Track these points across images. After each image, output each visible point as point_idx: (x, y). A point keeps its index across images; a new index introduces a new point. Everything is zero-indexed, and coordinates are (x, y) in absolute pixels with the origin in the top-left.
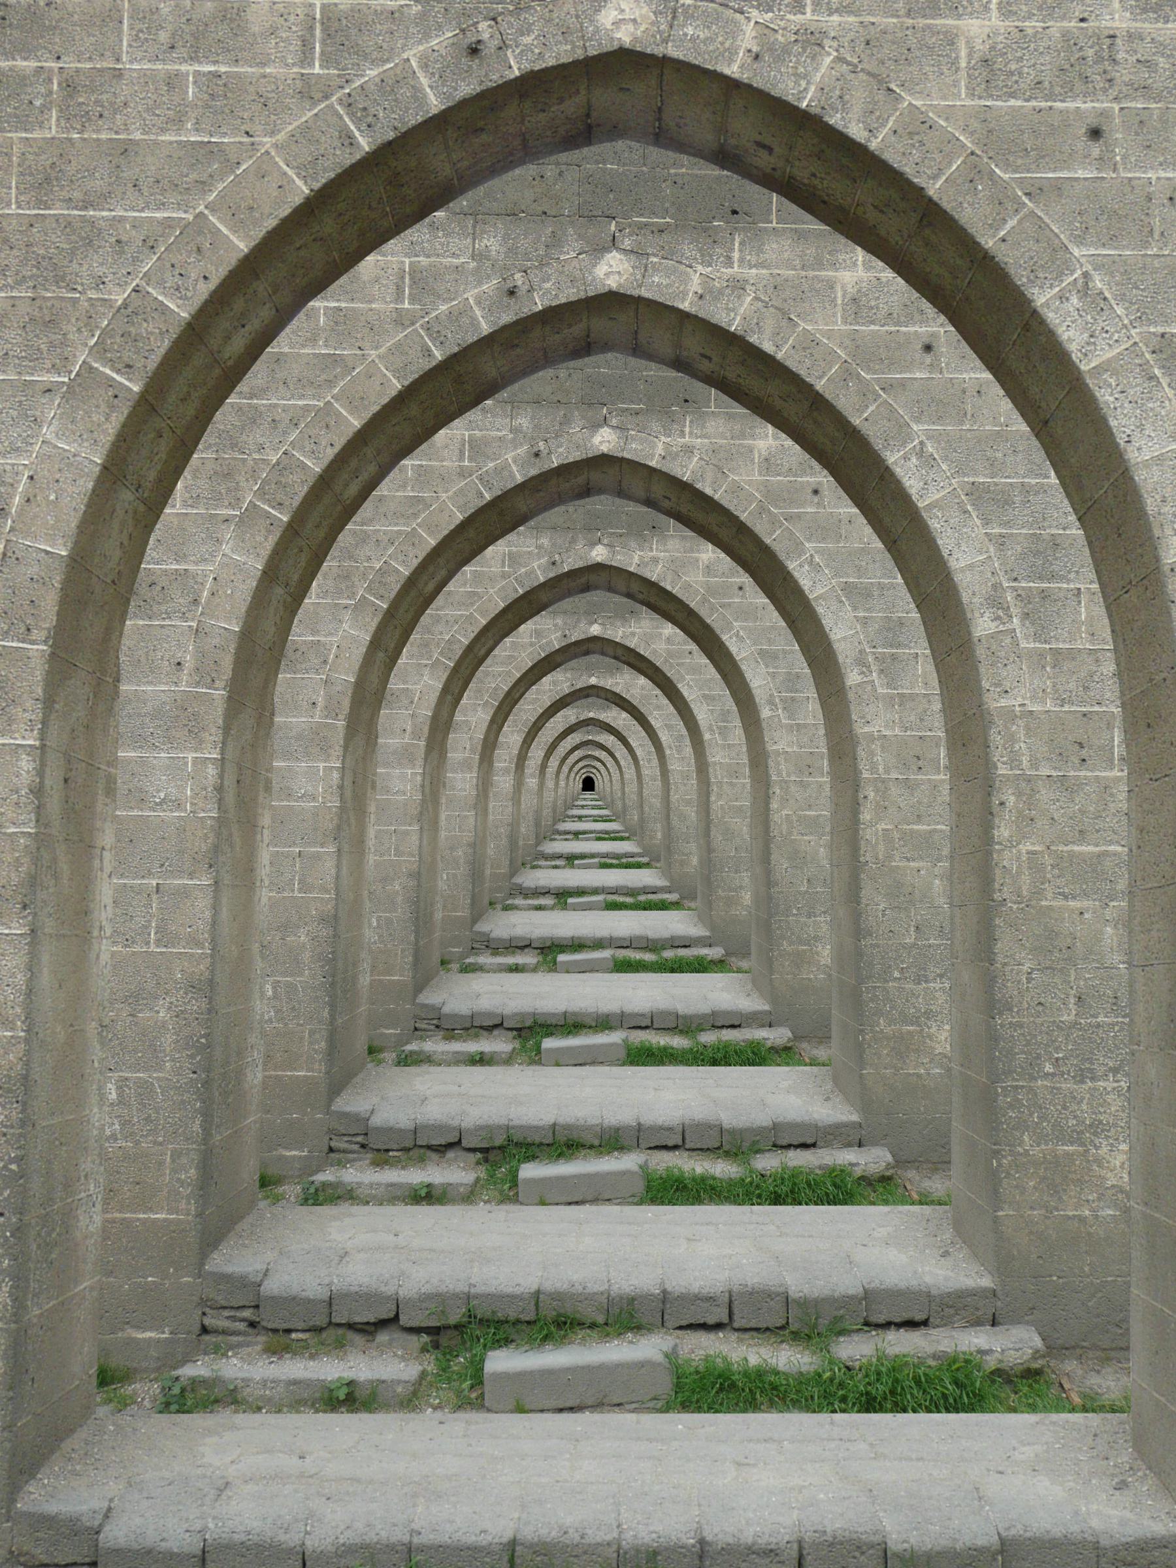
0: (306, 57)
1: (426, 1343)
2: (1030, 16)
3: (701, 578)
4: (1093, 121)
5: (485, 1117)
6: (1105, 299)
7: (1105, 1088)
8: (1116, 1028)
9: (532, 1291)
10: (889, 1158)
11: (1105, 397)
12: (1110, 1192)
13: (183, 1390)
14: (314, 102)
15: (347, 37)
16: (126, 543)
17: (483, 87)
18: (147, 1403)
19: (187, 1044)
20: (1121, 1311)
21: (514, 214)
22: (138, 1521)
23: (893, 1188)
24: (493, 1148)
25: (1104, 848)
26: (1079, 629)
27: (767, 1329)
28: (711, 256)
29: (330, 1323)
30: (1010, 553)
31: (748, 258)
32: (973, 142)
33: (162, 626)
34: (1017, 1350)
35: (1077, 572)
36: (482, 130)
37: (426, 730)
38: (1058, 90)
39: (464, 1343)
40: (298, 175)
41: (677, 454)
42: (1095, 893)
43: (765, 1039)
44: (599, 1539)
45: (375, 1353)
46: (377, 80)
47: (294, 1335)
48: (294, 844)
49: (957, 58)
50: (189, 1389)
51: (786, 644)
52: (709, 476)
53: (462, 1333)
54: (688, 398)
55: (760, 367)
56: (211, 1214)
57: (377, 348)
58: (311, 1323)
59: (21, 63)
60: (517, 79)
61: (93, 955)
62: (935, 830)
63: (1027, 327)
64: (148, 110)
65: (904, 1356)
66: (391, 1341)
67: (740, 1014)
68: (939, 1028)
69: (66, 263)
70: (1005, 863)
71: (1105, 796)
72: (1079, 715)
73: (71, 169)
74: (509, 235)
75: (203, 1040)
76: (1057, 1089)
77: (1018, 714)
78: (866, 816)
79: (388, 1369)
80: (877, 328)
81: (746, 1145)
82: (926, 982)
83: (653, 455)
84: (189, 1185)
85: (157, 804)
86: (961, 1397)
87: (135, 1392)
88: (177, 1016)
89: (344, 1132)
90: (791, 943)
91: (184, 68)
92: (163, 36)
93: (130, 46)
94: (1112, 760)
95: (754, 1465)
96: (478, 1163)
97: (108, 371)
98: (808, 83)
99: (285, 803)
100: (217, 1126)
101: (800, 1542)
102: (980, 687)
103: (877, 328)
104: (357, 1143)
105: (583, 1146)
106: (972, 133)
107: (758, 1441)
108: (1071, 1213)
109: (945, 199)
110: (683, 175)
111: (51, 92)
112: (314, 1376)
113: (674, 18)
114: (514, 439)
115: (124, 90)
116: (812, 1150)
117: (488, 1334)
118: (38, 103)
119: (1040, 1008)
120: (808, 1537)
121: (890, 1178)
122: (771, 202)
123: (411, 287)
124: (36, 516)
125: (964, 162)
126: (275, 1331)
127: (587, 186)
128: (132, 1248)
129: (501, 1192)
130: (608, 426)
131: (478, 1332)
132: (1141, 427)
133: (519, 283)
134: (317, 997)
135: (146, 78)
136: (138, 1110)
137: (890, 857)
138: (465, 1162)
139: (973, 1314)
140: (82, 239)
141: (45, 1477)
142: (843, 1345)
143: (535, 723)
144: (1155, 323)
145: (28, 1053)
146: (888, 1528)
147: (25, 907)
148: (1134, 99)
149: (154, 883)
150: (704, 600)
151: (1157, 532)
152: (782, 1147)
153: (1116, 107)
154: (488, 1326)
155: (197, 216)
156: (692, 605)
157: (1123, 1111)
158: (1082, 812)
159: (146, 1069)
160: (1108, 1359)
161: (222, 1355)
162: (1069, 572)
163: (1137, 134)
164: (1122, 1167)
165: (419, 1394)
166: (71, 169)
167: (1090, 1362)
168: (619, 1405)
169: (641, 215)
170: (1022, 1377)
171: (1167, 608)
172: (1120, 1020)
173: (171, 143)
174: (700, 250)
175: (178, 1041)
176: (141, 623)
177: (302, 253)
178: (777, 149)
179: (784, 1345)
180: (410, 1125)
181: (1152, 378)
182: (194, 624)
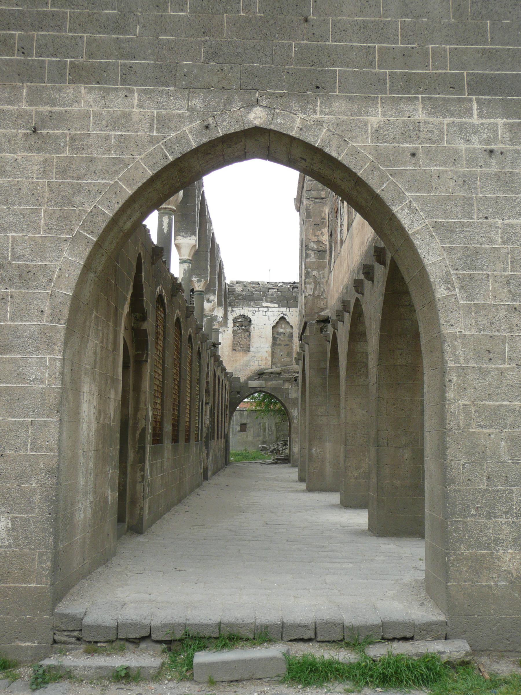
0: (151, 130)
1: (165, 648)
2: (392, 116)
3: (370, 144)
4: (413, 151)
5: (169, 617)
6: (417, 210)
7: (501, 522)
8: (507, 492)
9: (217, 622)
10: (468, 648)
11: (417, 242)
12: (503, 573)
13: (44, 672)
14: (154, 144)
15: (165, 123)
16: (91, 291)
17: (210, 139)
18: (26, 678)
19: (46, 500)
20: (509, 632)
21: (208, 88)
22: (96, 616)
23: (471, 670)
24: (175, 640)
25: (501, 403)
26: (488, 294)
27: (334, 641)
28: (306, 109)
29: (117, 638)
30: (454, 256)
31: (324, 110)
32: (373, 158)
33: (34, 293)
34: (457, 652)
35: (487, 266)
36: (210, 153)
37: (66, 311)
38: (401, 140)
39: (183, 648)
40: (149, 168)
41: (311, 127)
42: (496, 425)
43: (440, 653)
44: (249, 622)
45: (139, 653)
46: (175, 137)
47: (99, 644)
48: (28, 415)
49: (367, 130)
50: (47, 671)
51: (464, 217)
52: (335, 143)
53: (182, 643)
54: (318, 85)
55: (330, 164)
56: (58, 584)
57: (140, 155)
58: (108, 638)
59: (56, 131)
60: (221, 137)
61: (80, 428)
62: (502, 405)
63: (391, 219)
64: (99, 147)
65: (402, 655)
66: (147, 647)
67: (412, 625)
68: (505, 551)
69: (71, 198)
70: (452, 410)
71: (501, 377)
72: (488, 337)
73: (73, 167)
74: (206, 99)
75: (54, 498)
76: (477, 522)
77: (458, 336)
78: (451, 395)
79: (146, 661)
80: (388, 145)
81: (362, 638)
82: (495, 517)
83: (293, 128)
84: (47, 570)
85: (31, 381)
86: (429, 675)
87: (20, 673)
88: (41, 486)
89: (64, 628)
90: (469, 547)
91: (111, 133)
92: (104, 122)
93: (93, 126)
94: (504, 359)
95: (300, 597)
96: (164, 652)
97: (85, 234)
98: (318, 138)
99: (20, 385)
100: (61, 541)
101: (315, 623)
102: (440, 323)
103: (388, 145)
104: (74, 637)
105: (241, 639)
106: (372, 155)
107: (301, 589)
108: (484, 584)
109: (363, 176)
110: (292, 69)
111: (67, 141)
112: (109, 665)
113: (273, 116)
114: (190, 116)
115: (91, 140)
116: (411, 642)
117: (195, 644)
118: (62, 145)
119: (469, 482)
120: (318, 621)
121: (468, 663)
122: (336, 83)
123: (157, 124)
124: (61, 282)
125: (370, 164)
126: (90, 642)
127: (245, 74)
128: (19, 601)
129: (181, 673)
130: (260, 106)
131: (190, 643)
132: (429, 252)
133: (211, 122)
134: (44, 529)
135: (98, 136)
136: (22, 533)
137: (468, 425)
138: (154, 651)
139: (436, 634)
140: (77, 190)
141: (64, 601)
142: (372, 649)
143: (114, 221)
144: (433, 218)
145: (59, 460)
146: (345, 618)
147: (58, 412)
148: (426, 143)
149: (30, 420)
150: (373, 168)
151: (434, 287)
152: (389, 640)
153: (420, 146)
154: (196, 640)
155: (115, 182)
156: (360, 173)
157: (510, 533)
158: (490, 385)
159: (26, 513)
160: (503, 656)
161: (64, 654)
162: (483, 266)
163: (427, 155)
164: (510, 561)
165: (161, 674)
166: (73, 167)
167: (494, 658)
168: (260, 679)
169: (271, 89)
170: (460, 665)
171: (437, 312)
172: (509, 488)
173: (106, 158)
174: (300, 106)
175: (42, 499)
176: (23, 291)
177: (150, 194)
178: (308, 160)
179: (342, 649)
180: (114, 624)
181: (432, 236)
182: (50, 292)
